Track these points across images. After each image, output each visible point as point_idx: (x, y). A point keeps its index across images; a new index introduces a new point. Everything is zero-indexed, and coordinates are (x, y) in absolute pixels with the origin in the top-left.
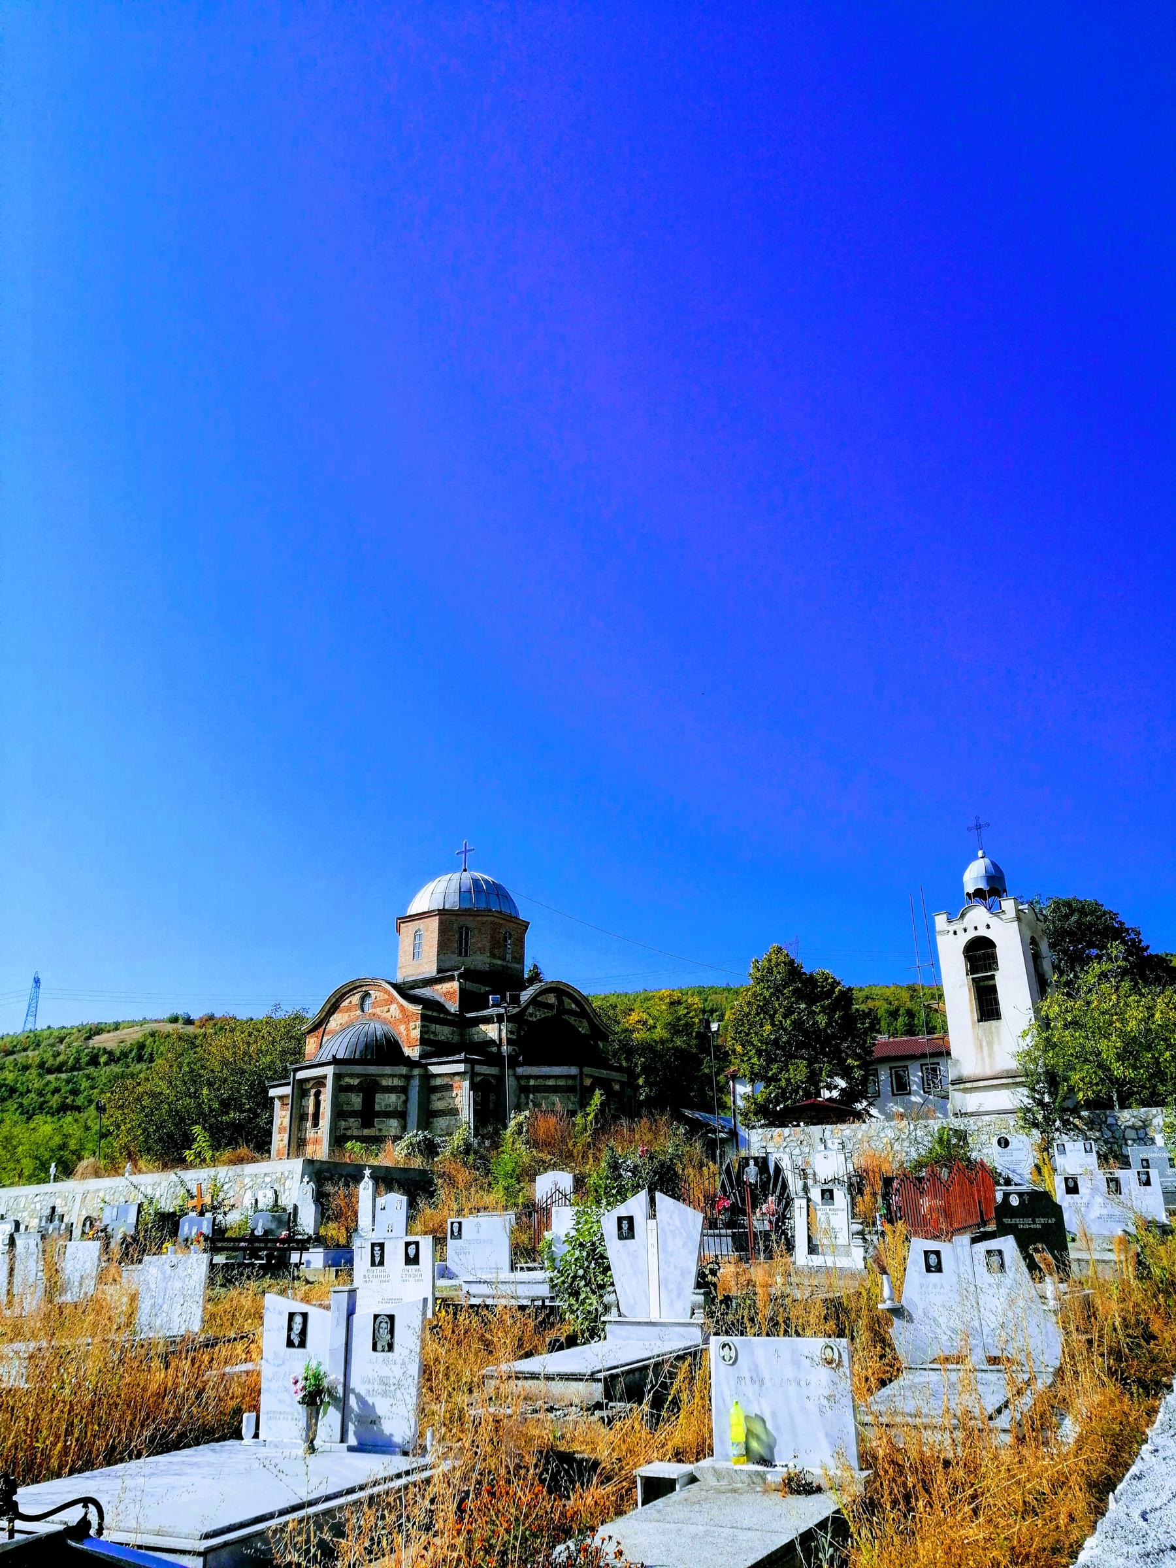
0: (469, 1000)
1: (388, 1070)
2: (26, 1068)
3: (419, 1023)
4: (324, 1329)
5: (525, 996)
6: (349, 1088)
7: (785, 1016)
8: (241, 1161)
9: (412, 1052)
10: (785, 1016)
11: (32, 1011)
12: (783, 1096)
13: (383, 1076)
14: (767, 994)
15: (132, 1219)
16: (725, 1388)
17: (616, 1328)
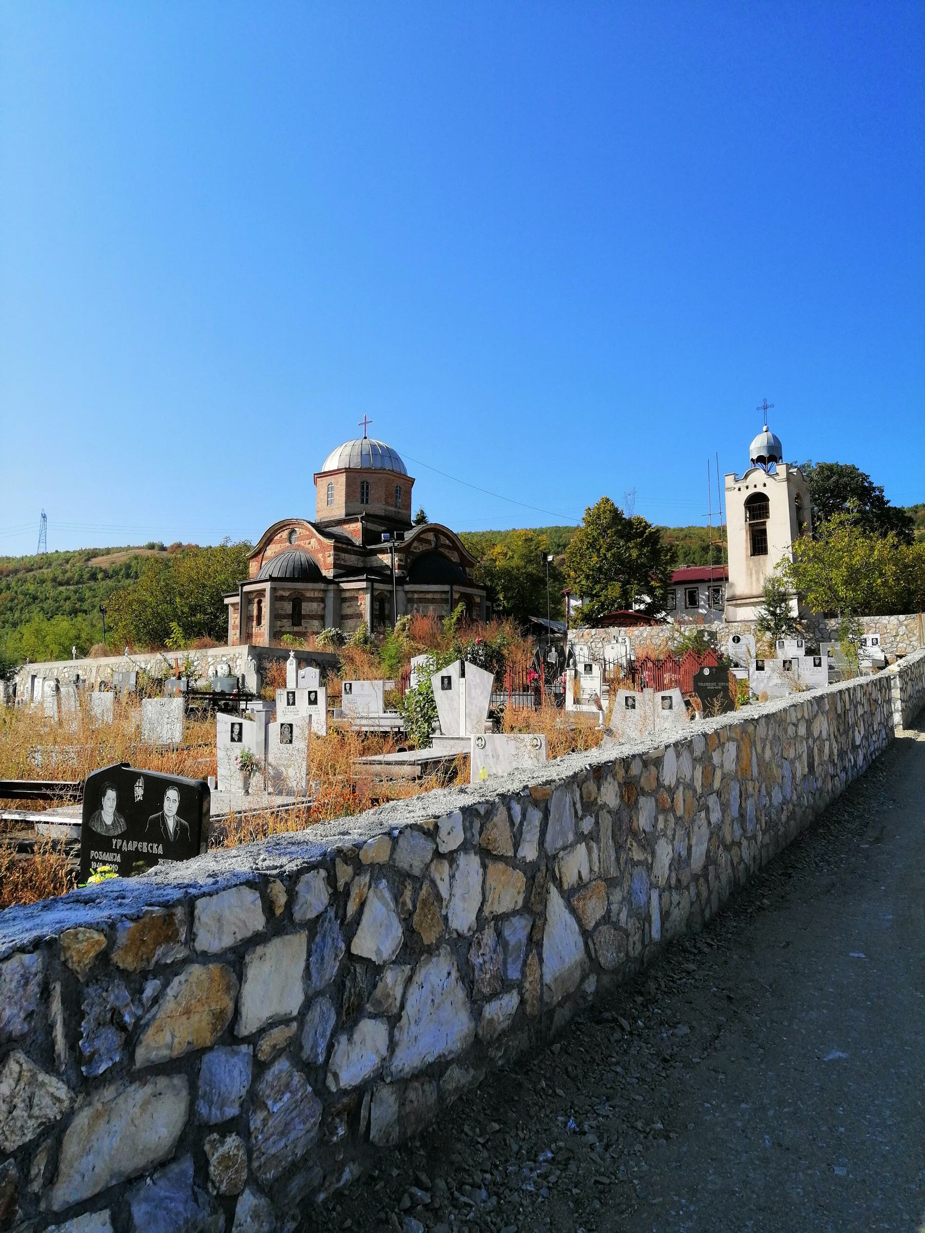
0: (370, 537)
1: (310, 585)
2: (43, 582)
3: (332, 552)
4: (252, 731)
5: (409, 535)
6: (282, 598)
7: (608, 550)
8: (205, 646)
9: (329, 573)
10: (608, 550)
11: (43, 537)
12: (602, 607)
13: (308, 590)
14: (595, 534)
15: (133, 682)
16: (478, 760)
17: (438, 741)
